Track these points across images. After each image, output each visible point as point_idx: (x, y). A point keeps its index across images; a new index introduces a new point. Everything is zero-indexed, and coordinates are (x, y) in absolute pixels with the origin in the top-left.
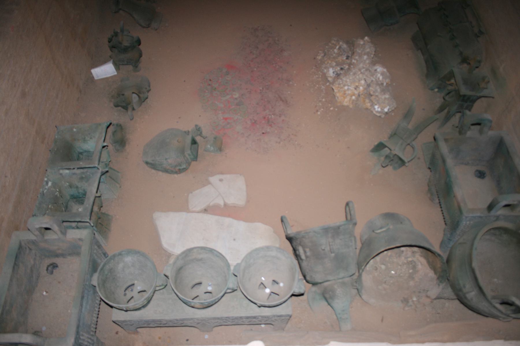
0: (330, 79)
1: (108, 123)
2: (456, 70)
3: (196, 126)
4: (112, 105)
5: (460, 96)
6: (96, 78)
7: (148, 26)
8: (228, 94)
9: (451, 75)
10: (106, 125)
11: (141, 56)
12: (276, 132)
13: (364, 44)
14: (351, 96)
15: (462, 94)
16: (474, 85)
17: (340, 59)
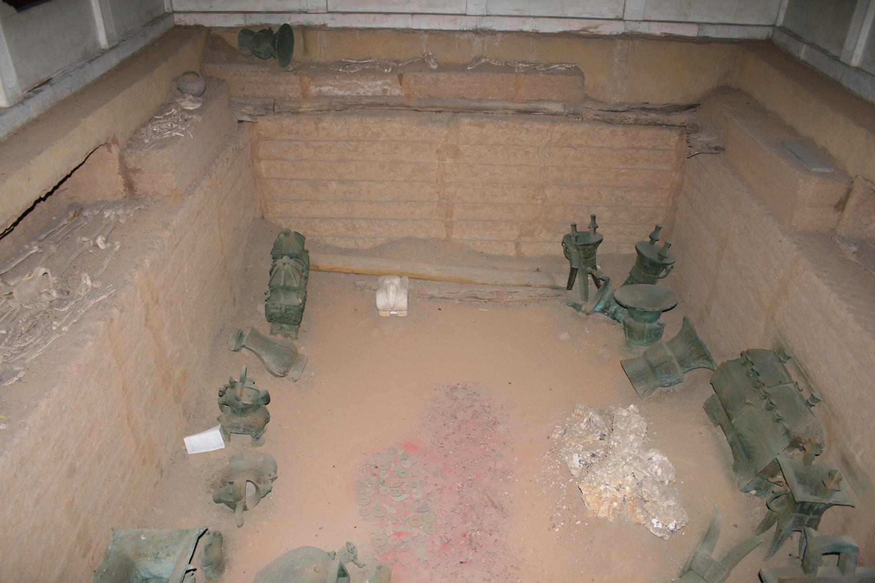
0: (574, 472)
1: (202, 531)
2: (783, 460)
3: (348, 544)
4: (210, 498)
5: (796, 503)
6: (190, 452)
7: (284, 375)
8: (404, 492)
9: (776, 468)
10: (198, 533)
11: (267, 421)
12: (484, 560)
13: (628, 416)
14: (611, 503)
15: (798, 500)
16: (818, 486)
17: (590, 438)
